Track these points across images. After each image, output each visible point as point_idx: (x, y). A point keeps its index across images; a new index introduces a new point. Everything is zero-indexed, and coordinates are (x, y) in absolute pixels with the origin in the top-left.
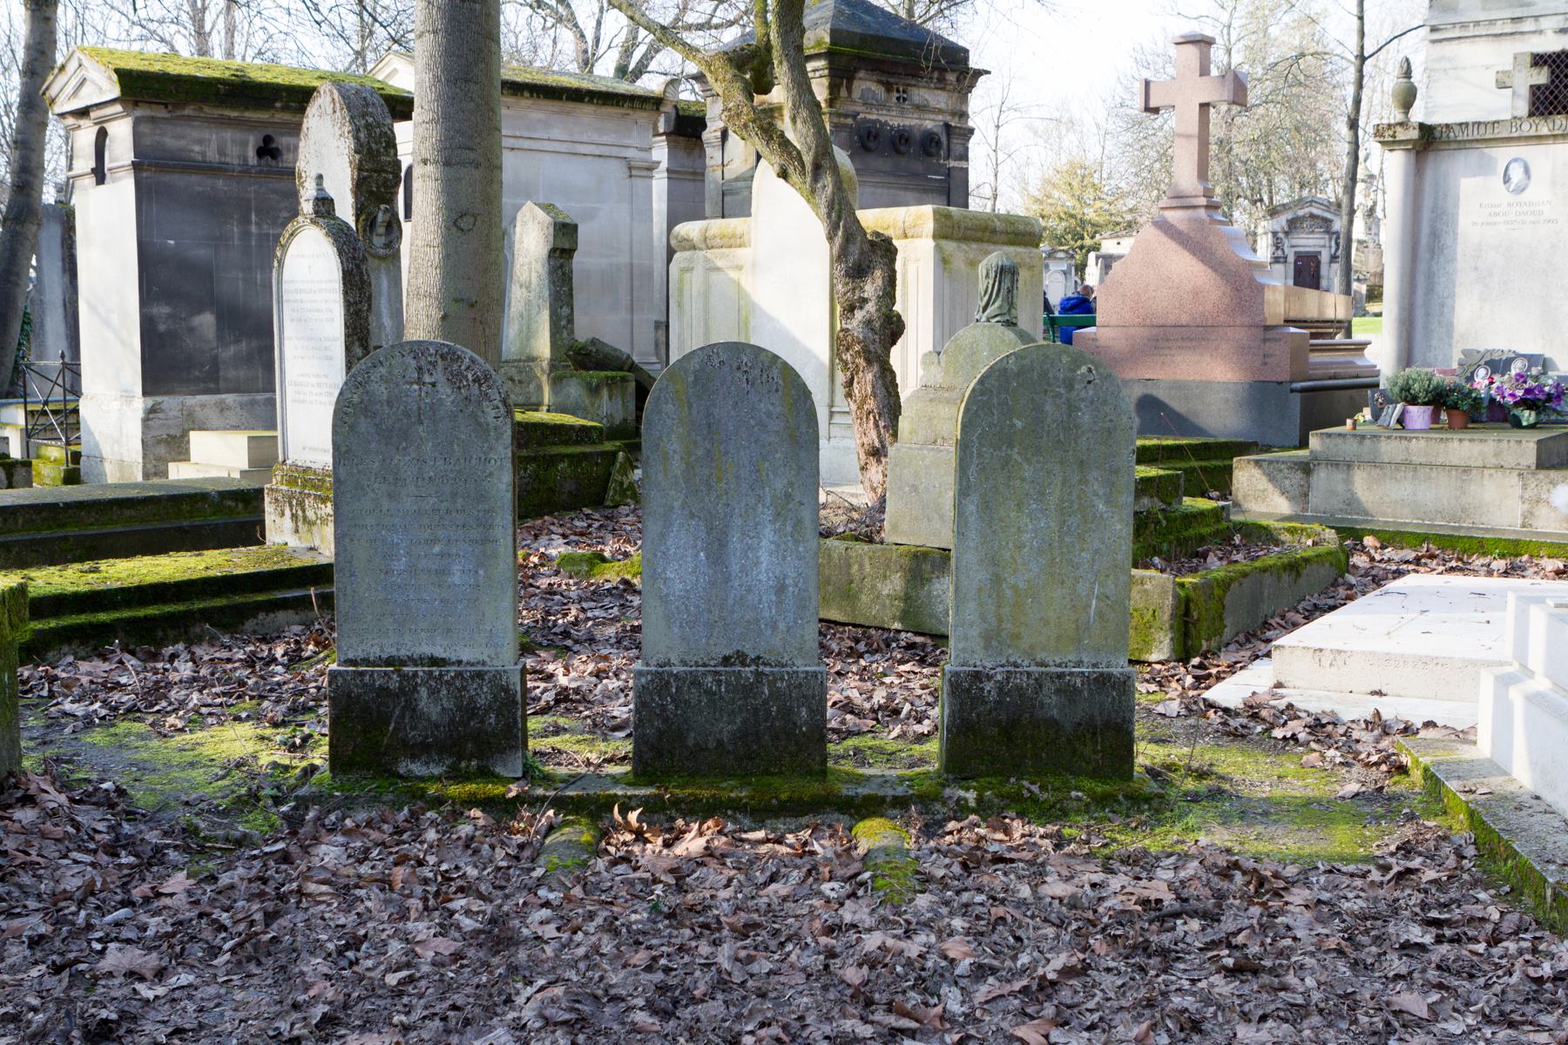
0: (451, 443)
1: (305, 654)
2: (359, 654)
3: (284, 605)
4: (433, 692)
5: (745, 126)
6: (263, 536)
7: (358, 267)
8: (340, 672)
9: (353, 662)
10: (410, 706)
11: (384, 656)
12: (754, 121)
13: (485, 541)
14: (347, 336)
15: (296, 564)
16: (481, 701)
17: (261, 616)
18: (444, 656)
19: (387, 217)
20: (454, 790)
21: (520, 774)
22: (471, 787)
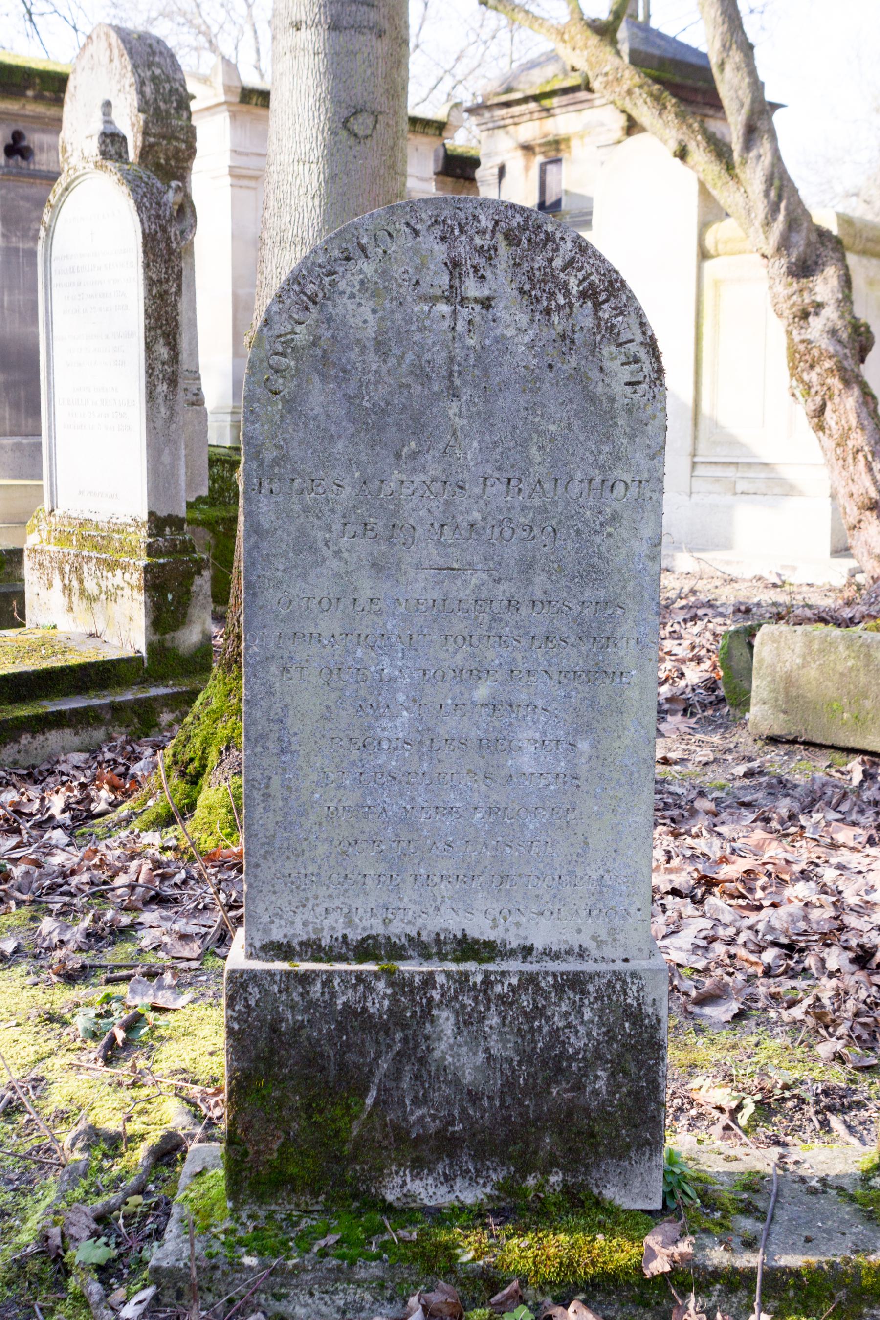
0: (524, 444)
1: (97, 808)
2: (297, 931)
3: (58, 721)
4: (468, 1022)
5: (629, 92)
6: (22, 615)
7: (164, 230)
8: (254, 976)
9: (283, 951)
10: (415, 1054)
11: (355, 936)
12: (641, 87)
13: (597, 673)
14: (148, 329)
15: (74, 659)
16: (577, 1042)
17: (25, 739)
18: (490, 935)
19: (179, 198)
20: (520, 1250)
21: (657, 1205)
22: (558, 1243)
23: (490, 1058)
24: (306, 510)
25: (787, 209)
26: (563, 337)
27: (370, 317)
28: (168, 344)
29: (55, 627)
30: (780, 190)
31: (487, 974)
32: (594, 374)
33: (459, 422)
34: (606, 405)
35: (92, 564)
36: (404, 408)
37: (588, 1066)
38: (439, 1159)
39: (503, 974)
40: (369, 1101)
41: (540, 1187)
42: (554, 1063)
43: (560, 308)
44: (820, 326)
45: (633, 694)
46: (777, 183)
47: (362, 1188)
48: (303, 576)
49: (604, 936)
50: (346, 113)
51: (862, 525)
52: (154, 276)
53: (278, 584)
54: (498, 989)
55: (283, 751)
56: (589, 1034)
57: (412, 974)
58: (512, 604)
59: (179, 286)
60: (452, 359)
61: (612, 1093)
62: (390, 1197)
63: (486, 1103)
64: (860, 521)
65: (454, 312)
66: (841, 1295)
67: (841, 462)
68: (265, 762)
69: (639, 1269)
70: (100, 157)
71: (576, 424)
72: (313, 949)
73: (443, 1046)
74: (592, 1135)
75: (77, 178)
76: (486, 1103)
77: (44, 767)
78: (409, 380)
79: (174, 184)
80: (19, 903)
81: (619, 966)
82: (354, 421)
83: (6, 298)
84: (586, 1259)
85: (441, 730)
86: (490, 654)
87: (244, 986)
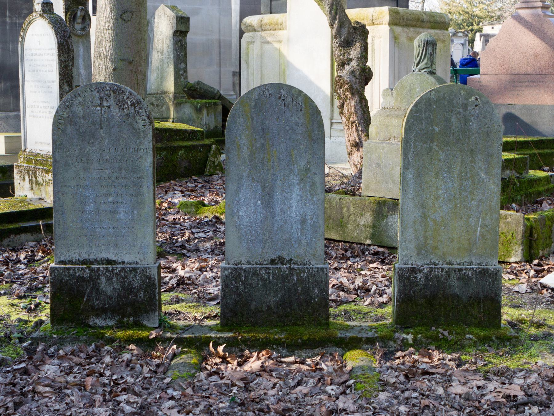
2: (66, 258)
3: (25, 230)
4: (109, 279)
6: (13, 192)
7: (66, 41)
8: (56, 268)
10: (96, 287)
11: (81, 259)
13: (138, 194)
14: (60, 80)
15: (32, 207)
16: (135, 284)
17: (12, 237)
18: (114, 259)
19: (83, 13)
20: (120, 334)
21: (157, 325)
22: (130, 332)
23: (114, 288)
24: (67, 156)
25: (339, 18)
26: (127, 115)
27: (81, 111)
28: (68, 85)
29: (26, 196)
30: (337, 10)
31: (113, 268)
32: (135, 123)
33: (103, 135)
34: (138, 131)
35: (40, 171)
36: (90, 132)
37: (139, 290)
38: (102, 314)
39: (117, 267)
40: (85, 299)
41: (128, 321)
42: (129, 290)
43: (126, 108)
44: (348, 70)
45: (147, 199)
46: (335, 7)
47: (84, 321)
48: (67, 172)
49: (142, 259)
50: (121, 13)
51: (352, 153)
52: (62, 59)
53: (61, 174)
54: (116, 271)
55: (63, 214)
56: (138, 282)
57: (95, 268)
58: (117, 178)
59: (73, 63)
60: (101, 120)
61: (144, 297)
62: (91, 324)
63: (113, 300)
64: (351, 151)
65: (101, 109)
66: (198, 344)
67: (347, 127)
68: (59, 216)
69: (148, 337)
70: (41, 12)
71: (131, 135)
72: (71, 262)
73: (103, 286)
74: (140, 308)
75: (32, 20)
76: (113, 300)
77: (19, 247)
78: (91, 125)
79: (80, 7)
80: (7, 282)
81: (146, 266)
82: (78, 135)
83: (11, 46)
84: (136, 335)
85: (101, 209)
86: (112, 190)
87: (54, 271)
